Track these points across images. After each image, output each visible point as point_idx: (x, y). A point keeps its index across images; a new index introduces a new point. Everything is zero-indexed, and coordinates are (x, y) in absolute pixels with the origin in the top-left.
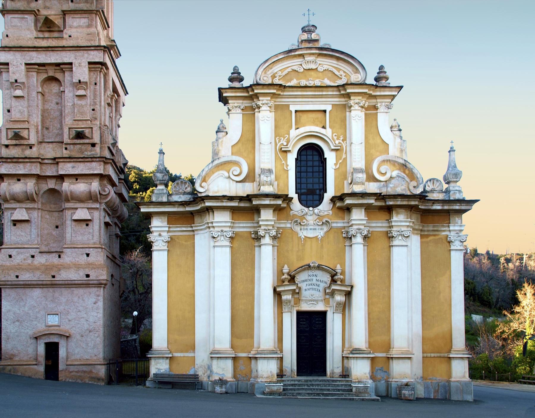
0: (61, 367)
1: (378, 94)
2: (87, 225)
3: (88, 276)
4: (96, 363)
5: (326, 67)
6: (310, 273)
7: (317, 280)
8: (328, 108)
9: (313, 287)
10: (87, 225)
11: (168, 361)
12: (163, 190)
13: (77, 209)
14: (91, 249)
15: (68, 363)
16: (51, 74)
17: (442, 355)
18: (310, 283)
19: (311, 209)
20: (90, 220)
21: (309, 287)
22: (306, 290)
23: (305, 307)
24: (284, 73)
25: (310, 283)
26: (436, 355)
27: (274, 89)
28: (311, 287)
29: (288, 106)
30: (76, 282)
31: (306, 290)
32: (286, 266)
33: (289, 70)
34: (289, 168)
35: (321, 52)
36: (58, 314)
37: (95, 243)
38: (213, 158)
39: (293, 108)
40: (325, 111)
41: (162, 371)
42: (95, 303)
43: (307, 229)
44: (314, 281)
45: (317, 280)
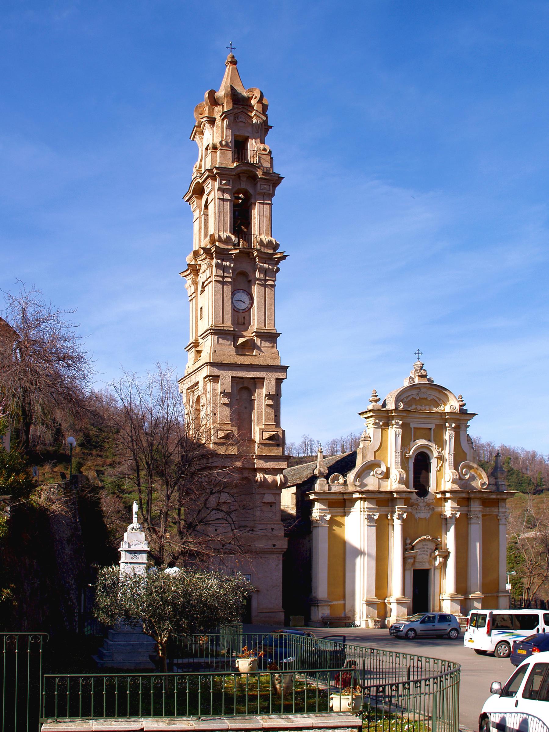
0: (254, 613)
1: (462, 418)
2: (271, 506)
3: (274, 545)
4: (278, 611)
5: (432, 397)
6: (424, 543)
7: (427, 548)
8: (433, 427)
9: (424, 553)
10: (271, 506)
11: (329, 607)
12: (324, 481)
13: (264, 494)
14: (276, 525)
15: (259, 611)
16: (245, 385)
17: (493, 594)
18: (423, 550)
19: (422, 498)
20: (274, 503)
21: (421, 553)
22: (419, 555)
23: (419, 567)
24: (408, 399)
25: (423, 550)
26: (489, 595)
27: (405, 413)
28: (423, 552)
29: (409, 424)
30: (266, 550)
31: (419, 555)
32: (408, 538)
33: (411, 397)
34: (410, 469)
35: (431, 387)
36: (250, 575)
37: (277, 521)
38: (363, 460)
39: (412, 426)
40: (430, 429)
41: (325, 615)
42: (277, 566)
43: (420, 512)
44: (426, 549)
45: (427, 548)
